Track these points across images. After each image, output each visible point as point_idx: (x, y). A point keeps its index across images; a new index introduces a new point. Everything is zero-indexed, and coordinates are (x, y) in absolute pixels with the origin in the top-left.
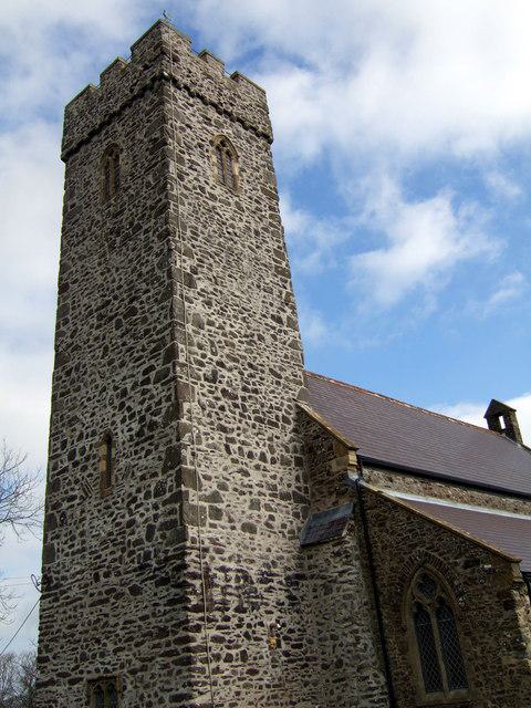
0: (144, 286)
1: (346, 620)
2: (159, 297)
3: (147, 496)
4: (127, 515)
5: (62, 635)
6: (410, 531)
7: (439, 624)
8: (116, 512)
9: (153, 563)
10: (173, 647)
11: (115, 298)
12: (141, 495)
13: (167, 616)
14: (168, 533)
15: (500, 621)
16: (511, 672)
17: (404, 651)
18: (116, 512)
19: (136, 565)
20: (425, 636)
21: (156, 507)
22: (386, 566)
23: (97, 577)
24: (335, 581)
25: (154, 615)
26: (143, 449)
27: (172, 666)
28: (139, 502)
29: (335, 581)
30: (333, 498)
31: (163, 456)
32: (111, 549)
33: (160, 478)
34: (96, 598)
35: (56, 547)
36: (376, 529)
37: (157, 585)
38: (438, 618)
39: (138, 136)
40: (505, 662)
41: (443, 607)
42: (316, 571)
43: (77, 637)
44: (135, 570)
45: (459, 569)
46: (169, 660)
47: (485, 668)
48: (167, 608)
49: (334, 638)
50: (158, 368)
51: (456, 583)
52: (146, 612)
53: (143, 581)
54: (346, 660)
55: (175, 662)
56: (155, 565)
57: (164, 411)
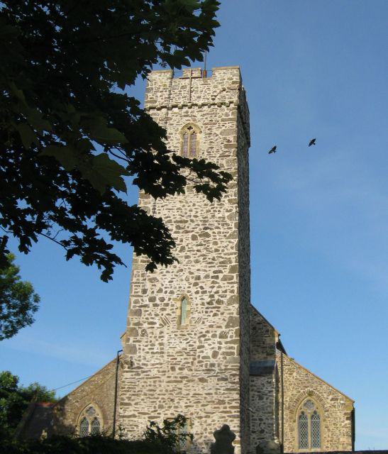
0: (216, 224)
1: (269, 413)
2: (228, 235)
3: (214, 336)
4: (197, 342)
5: (143, 393)
6: (306, 380)
7: (312, 422)
8: (190, 339)
9: (217, 369)
10: (228, 409)
11: (192, 221)
12: (210, 335)
13: (225, 395)
14: (228, 357)
15: (343, 424)
16: (343, 444)
17: (292, 430)
18: (190, 339)
19: (204, 368)
20: (303, 426)
21: (220, 343)
22: (290, 394)
23: (173, 369)
24: (266, 395)
25: (216, 393)
26: (212, 311)
27: (227, 418)
28: (207, 338)
29: (266, 395)
30: (265, 355)
31: (226, 319)
32: (185, 356)
33: (224, 329)
34: (172, 379)
35: (138, 347)
36: (288, 375)
37: (218, 380)
38: (312, 419)
39: (214, 131)
40: (341, 440)
41: (315, 415)
42: (255, 388)
43: (156, 396)
44: (203, 370)
45: (329, 401)
46: (225, 415)
47: (331, 441)
48: (226, 392)
49: (261, 420)
50: (225, 274)
51: (326, 406)
52: (211, 391)
53: (209, 377)
54: (266, 430)
55: (228, 416)
56: (217, 371)
57: (228, 297)
